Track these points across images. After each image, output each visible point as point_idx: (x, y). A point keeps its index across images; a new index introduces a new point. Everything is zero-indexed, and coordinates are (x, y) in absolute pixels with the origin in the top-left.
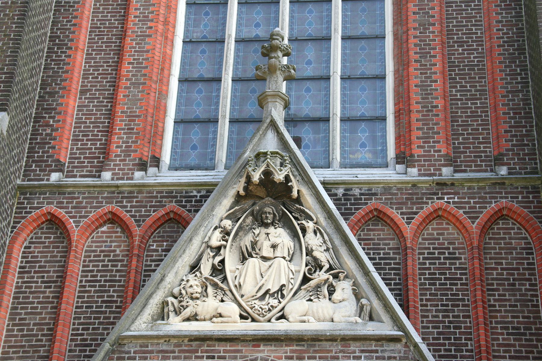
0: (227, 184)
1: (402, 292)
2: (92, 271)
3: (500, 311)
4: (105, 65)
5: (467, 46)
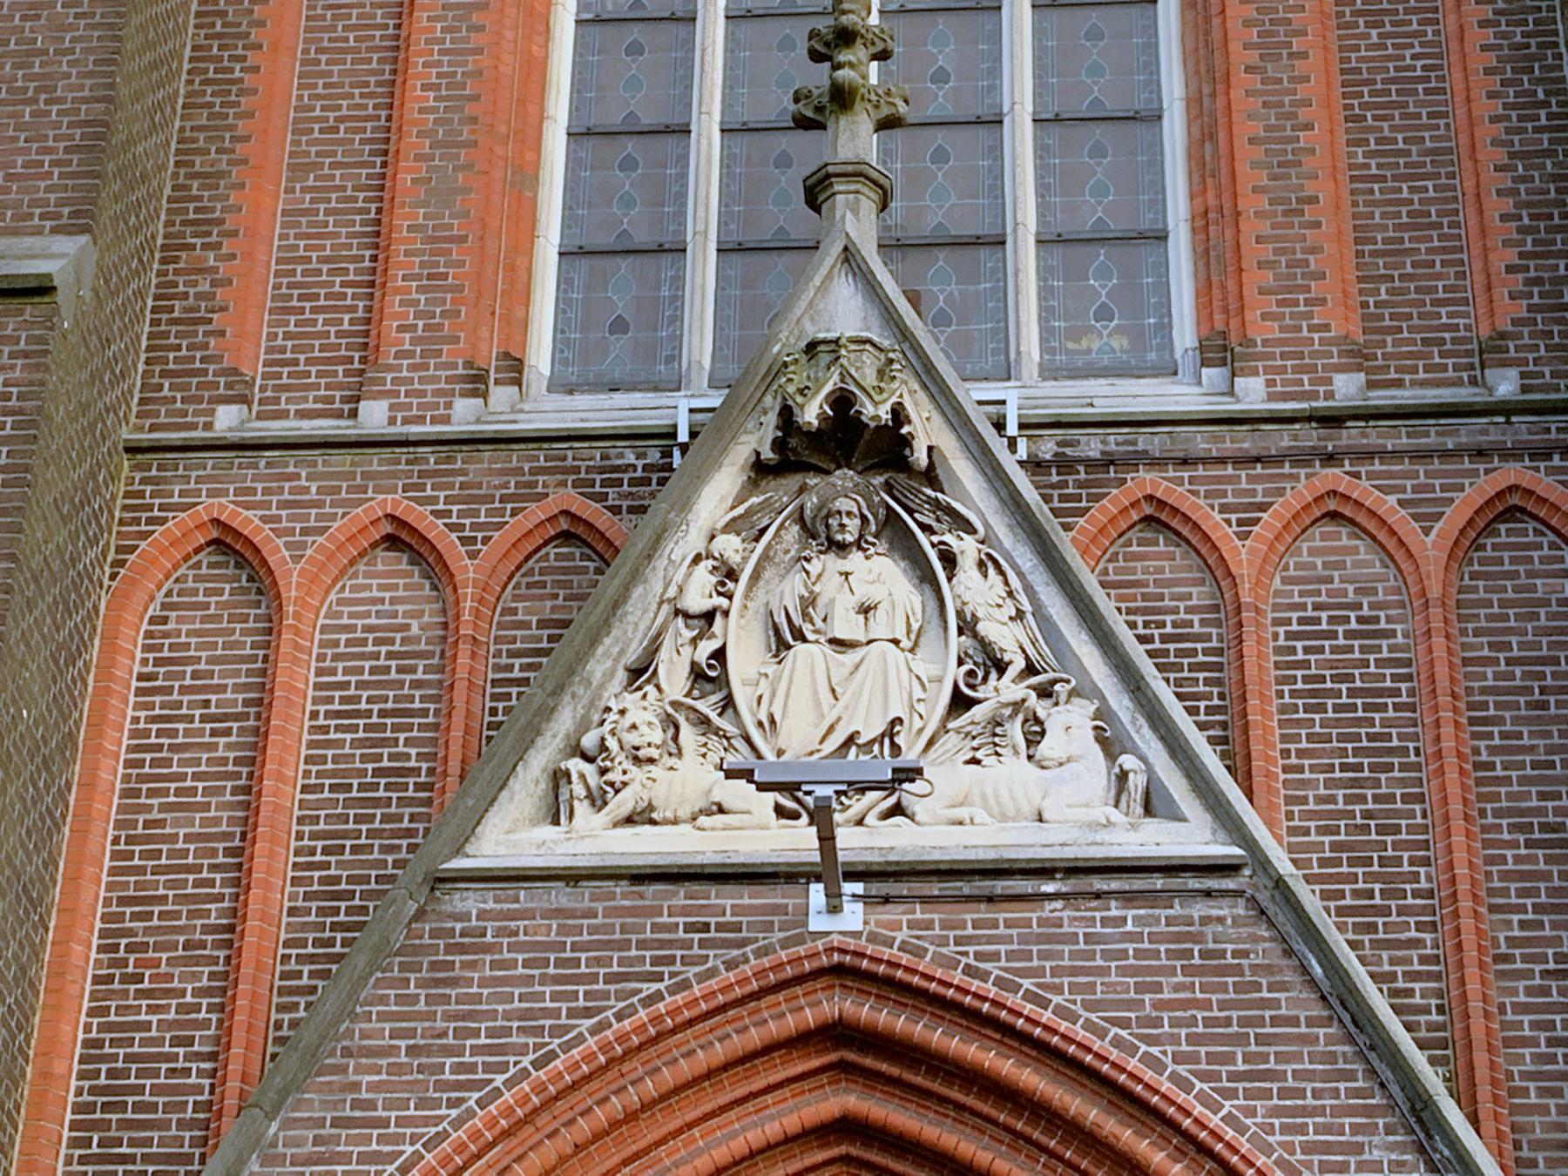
0: (710, 432)
1: (1229, 733)
2: (344, 685)
3: (1507, 781)
4: (357, 91)
5: (1393, 24)
